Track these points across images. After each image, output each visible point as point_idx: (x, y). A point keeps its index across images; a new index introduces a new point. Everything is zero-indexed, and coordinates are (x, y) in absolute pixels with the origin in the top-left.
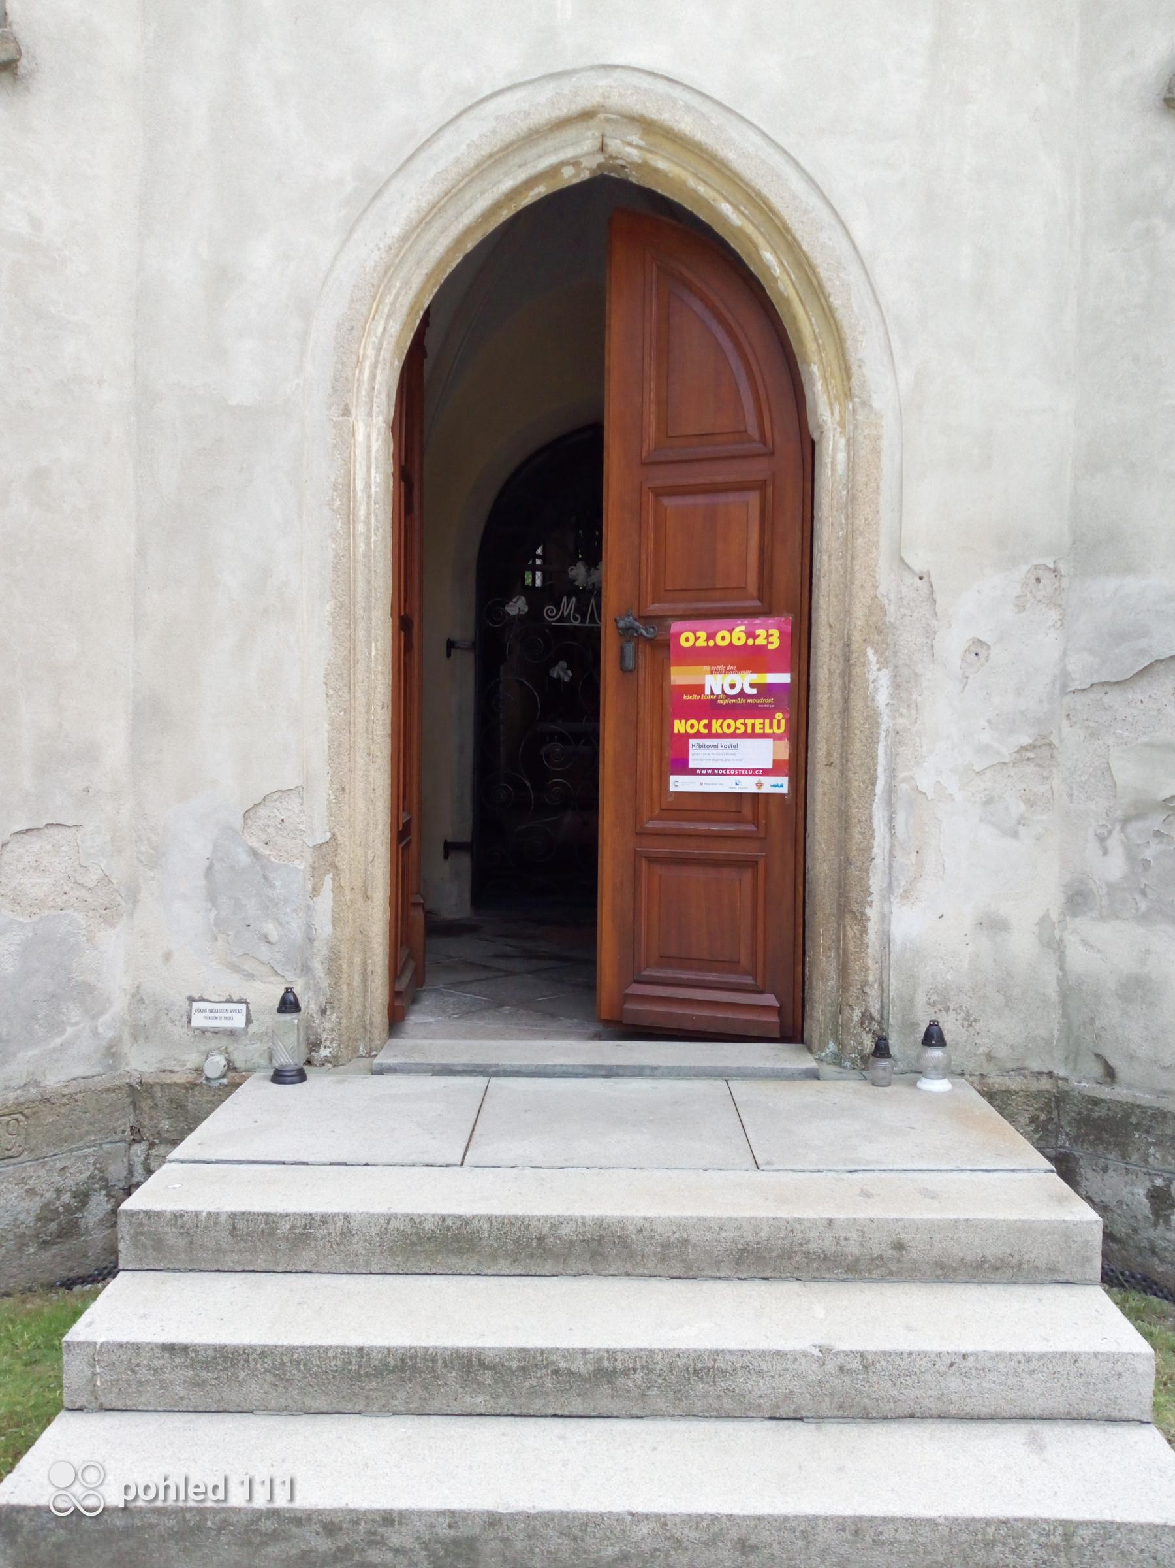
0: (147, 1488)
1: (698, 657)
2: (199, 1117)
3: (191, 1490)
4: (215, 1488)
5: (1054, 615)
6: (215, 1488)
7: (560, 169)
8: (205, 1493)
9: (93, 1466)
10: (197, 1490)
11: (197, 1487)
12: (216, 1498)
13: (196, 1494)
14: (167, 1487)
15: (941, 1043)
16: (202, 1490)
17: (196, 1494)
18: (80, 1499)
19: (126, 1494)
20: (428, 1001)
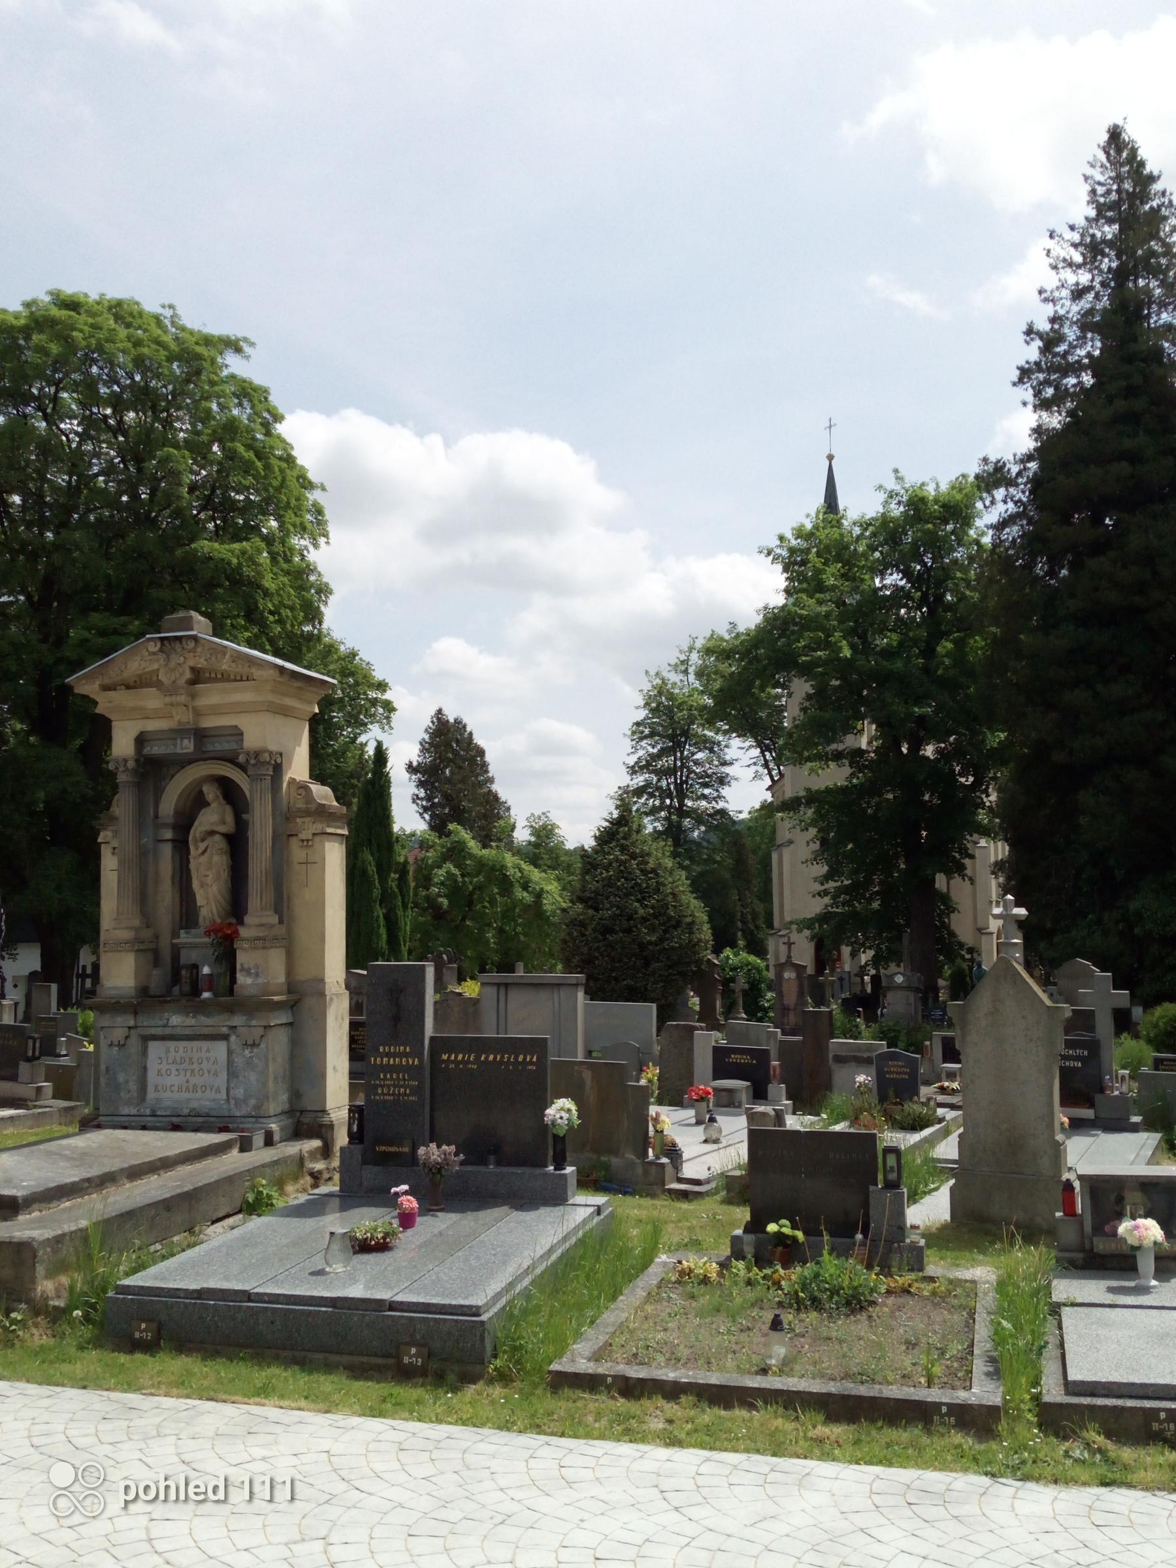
0: (147, 1488)
1: (905, 1073)
2: (371, 782)
3: (191, 1490)
4: (216, 1488)
5: (1092, 213)
6: (216, 1488)
7: (1097, 215)
8: (205, 1493)
9: (59, 1496)
10: (197, 1490)
11: (197, 1487)
12: (215, 1498)
13: (196, 1494)
14: (167, 1487)
15: (1084, 175)
16: (202, 1489)
17: (196, 1494)
18: (81, 1499)
19: (126, 1494)
20: (133, 992)
